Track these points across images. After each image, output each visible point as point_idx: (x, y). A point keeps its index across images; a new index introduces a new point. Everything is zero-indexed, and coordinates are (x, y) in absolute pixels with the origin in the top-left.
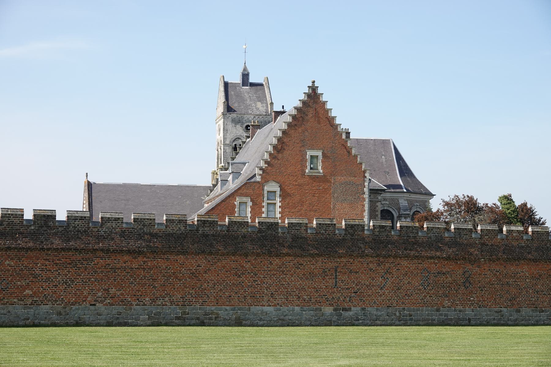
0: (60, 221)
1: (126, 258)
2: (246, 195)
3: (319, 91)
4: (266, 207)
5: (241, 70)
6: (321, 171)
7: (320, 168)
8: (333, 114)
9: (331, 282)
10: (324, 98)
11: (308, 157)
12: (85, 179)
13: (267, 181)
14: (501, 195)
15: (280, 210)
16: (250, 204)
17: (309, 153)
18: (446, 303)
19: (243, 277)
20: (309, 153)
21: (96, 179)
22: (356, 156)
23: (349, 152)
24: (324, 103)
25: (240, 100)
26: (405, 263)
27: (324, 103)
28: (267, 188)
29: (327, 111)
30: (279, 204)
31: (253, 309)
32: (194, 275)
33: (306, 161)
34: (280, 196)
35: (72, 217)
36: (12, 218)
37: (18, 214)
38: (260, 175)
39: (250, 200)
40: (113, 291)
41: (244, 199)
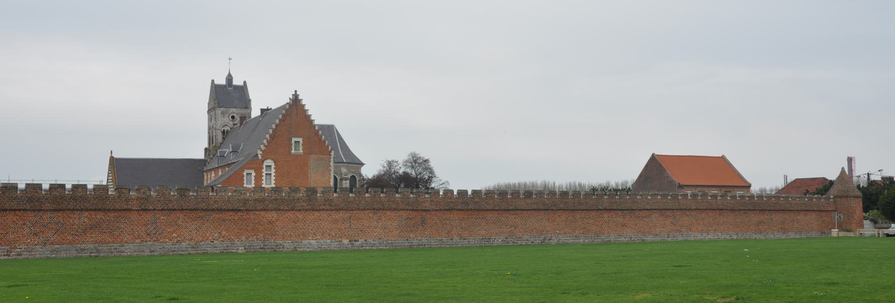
0: (22, 190)
1: (231, 213)
5: (227, 74)
8: (309, 113)
9: (348, 225)
14: (424, 154)
16: (254, 174)
17: (294, 140)
18: (412, 236)
19: (298, 224)
20: (294, 140)
21: (116, 156)
22: (324, 142)
23: (320, 139)
24: (304, 105)
25: (228, 97)
26: (388, 213)
27: (304, 105)
29: (306, 111)
30: (273, 174)
31: (304, 242)
32: (270, 222)
35: (97, 188)
36: (10, 188)
37: (14, 187)
40: (224, 233)
41: (249, 171)
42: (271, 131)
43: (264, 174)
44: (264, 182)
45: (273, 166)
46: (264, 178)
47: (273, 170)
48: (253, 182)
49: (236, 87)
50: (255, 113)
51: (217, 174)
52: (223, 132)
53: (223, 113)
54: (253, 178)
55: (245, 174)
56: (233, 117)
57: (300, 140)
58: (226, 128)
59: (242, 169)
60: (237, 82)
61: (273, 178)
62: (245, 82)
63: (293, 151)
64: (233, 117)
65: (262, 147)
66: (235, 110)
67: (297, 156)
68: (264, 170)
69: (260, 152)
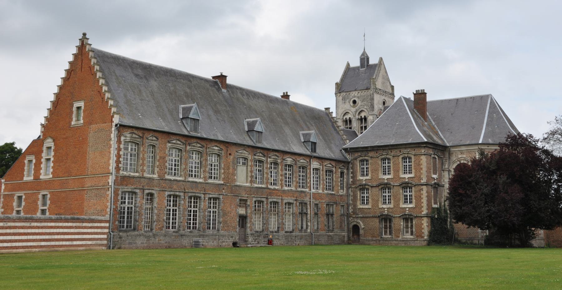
28: (46, 145)
33: (72, 112)
44: (42, 171)
56: (354, 102)
58: (347, 117)
64: (354, 102)
66: (355, 93)
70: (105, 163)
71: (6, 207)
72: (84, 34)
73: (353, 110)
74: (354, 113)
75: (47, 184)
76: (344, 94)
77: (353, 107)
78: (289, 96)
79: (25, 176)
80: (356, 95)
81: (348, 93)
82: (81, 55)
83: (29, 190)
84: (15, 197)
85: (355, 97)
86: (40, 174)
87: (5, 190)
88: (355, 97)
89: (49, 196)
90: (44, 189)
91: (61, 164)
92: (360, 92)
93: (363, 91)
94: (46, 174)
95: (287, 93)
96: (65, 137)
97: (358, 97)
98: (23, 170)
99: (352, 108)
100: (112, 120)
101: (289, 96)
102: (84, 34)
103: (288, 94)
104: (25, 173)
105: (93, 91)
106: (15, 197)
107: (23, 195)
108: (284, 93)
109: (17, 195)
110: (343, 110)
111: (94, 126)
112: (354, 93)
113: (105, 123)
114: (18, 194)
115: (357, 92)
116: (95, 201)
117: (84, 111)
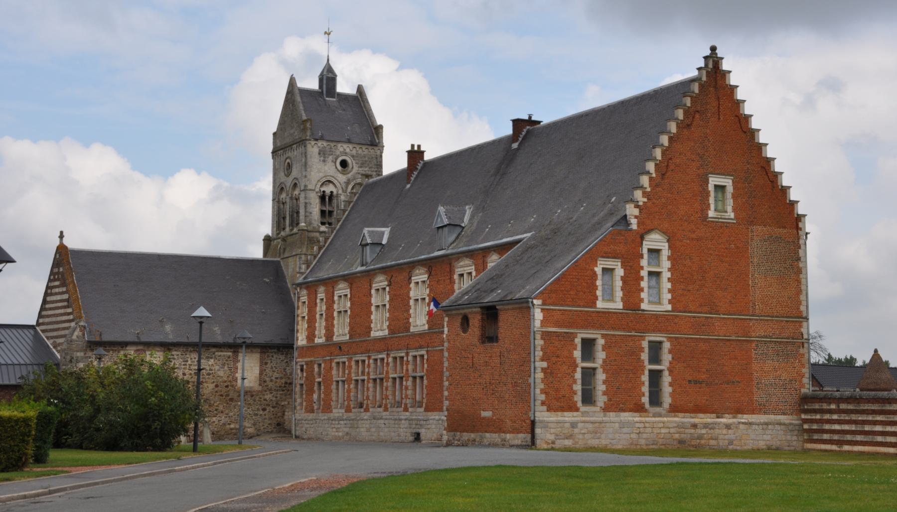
2: (615, 256)
3: (725, 66)
4: (646, 279)
6: (732, 215)
7: (729, 209)
10: (733, 80)
11: (711, 188)
12: (57, 242)
13: (649, 231)
15: (669, 296)
16: (620, 272)
21: (72, 243)
24: (793, 204)
27: (793, 204)
28: (647, 245)
29: (739, 103)
30: (666, 275)
33: (708, 193)
34: (669, 258)
38: (636, 217)
39: (619, 264)
42: (658, 153)
43: (644, 273)
44: (644, 295)
45: (666, 252)
46: (644, 284)
47: (666, 264)
48: (619, 294)
49: (344, 97)
50: (394, 161)
51: (481, 267)
52: (323, 198)
53: (322, 153)
54: (619, 284)
55: (598, 270)
56: (344, 164)
57: (727, 182)
58: (328, 189)
59: (592, 257)
60: (344, 87)
61: (666, 285)
62: (360, 89)
63: (711, 213)
64: (344, 164)
65: (638, 195)
66: (348, 148)
67: (720, 226)
68: (644, 262)
69: (631, 211)
70: (789, 298)
71: (554, 359)
72: (713, 49)
73: (342, 178)
74: (344, 185)
75: (658, 322)
76: (325, 144)
77: (343, 173)
78: (423, 152)
79: (600, 298)
80: (348, 150)
81: (332, 144)
82: (715, 87)
83: (613, 329)
84: (578, 341)
85: (346, 154)
86: (642, 300)
87: (544, 323)
88: (346, 154)
89: (667, 346)
90: (654, 331)
91: (690, 288)
92: (358, 147)
93: (364, 147)
94: (657, 299)
95: (419, 146)
96: (694, 236)
97: (353, 156)
98: (595, 288)
99: (340, 175)
100: (797, 225)
101: (423, 152)
102: (713, 49)
103: (422, 149)
104: (599, 293)
105: (749, 163)
106: (578, 341)
107: (599, 336)
108: (413, 146)
109: (647, 339)
110: (321, 175)
111: (760, 228)
112: (345, 146)
113: (784, 227)
114: (581, 335)
115: (351, 146)
116: (777, 364)
117: (734, 196)
